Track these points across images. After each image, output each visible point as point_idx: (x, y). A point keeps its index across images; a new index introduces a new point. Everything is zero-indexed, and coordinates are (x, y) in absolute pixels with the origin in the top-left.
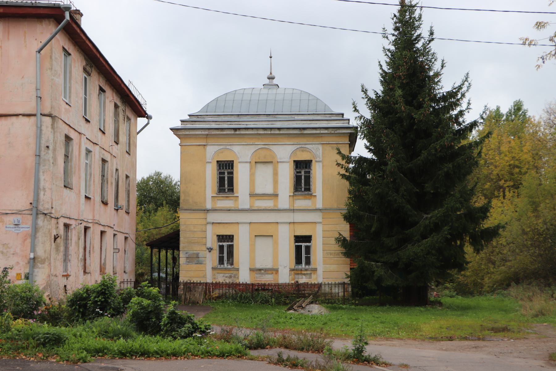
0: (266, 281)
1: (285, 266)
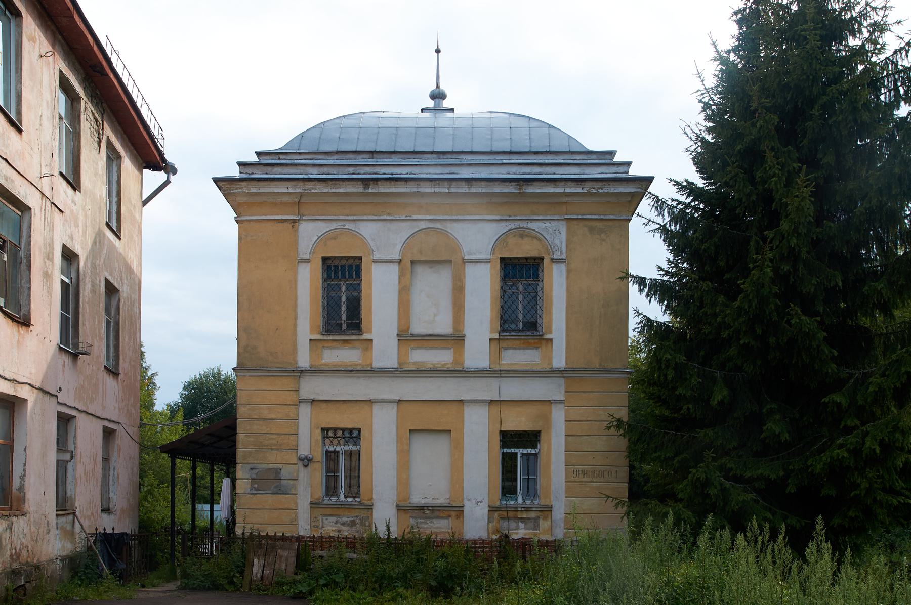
1: (478, 500)
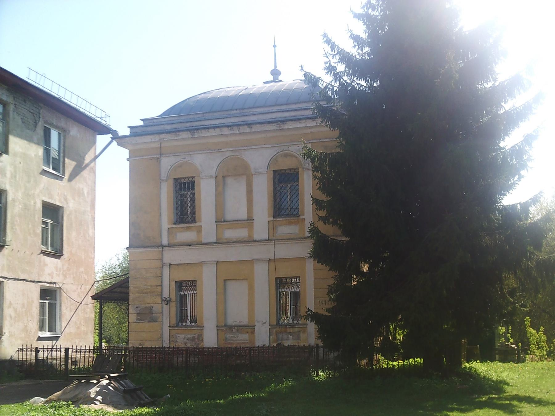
0: (239, 343)
1: (264, 322)
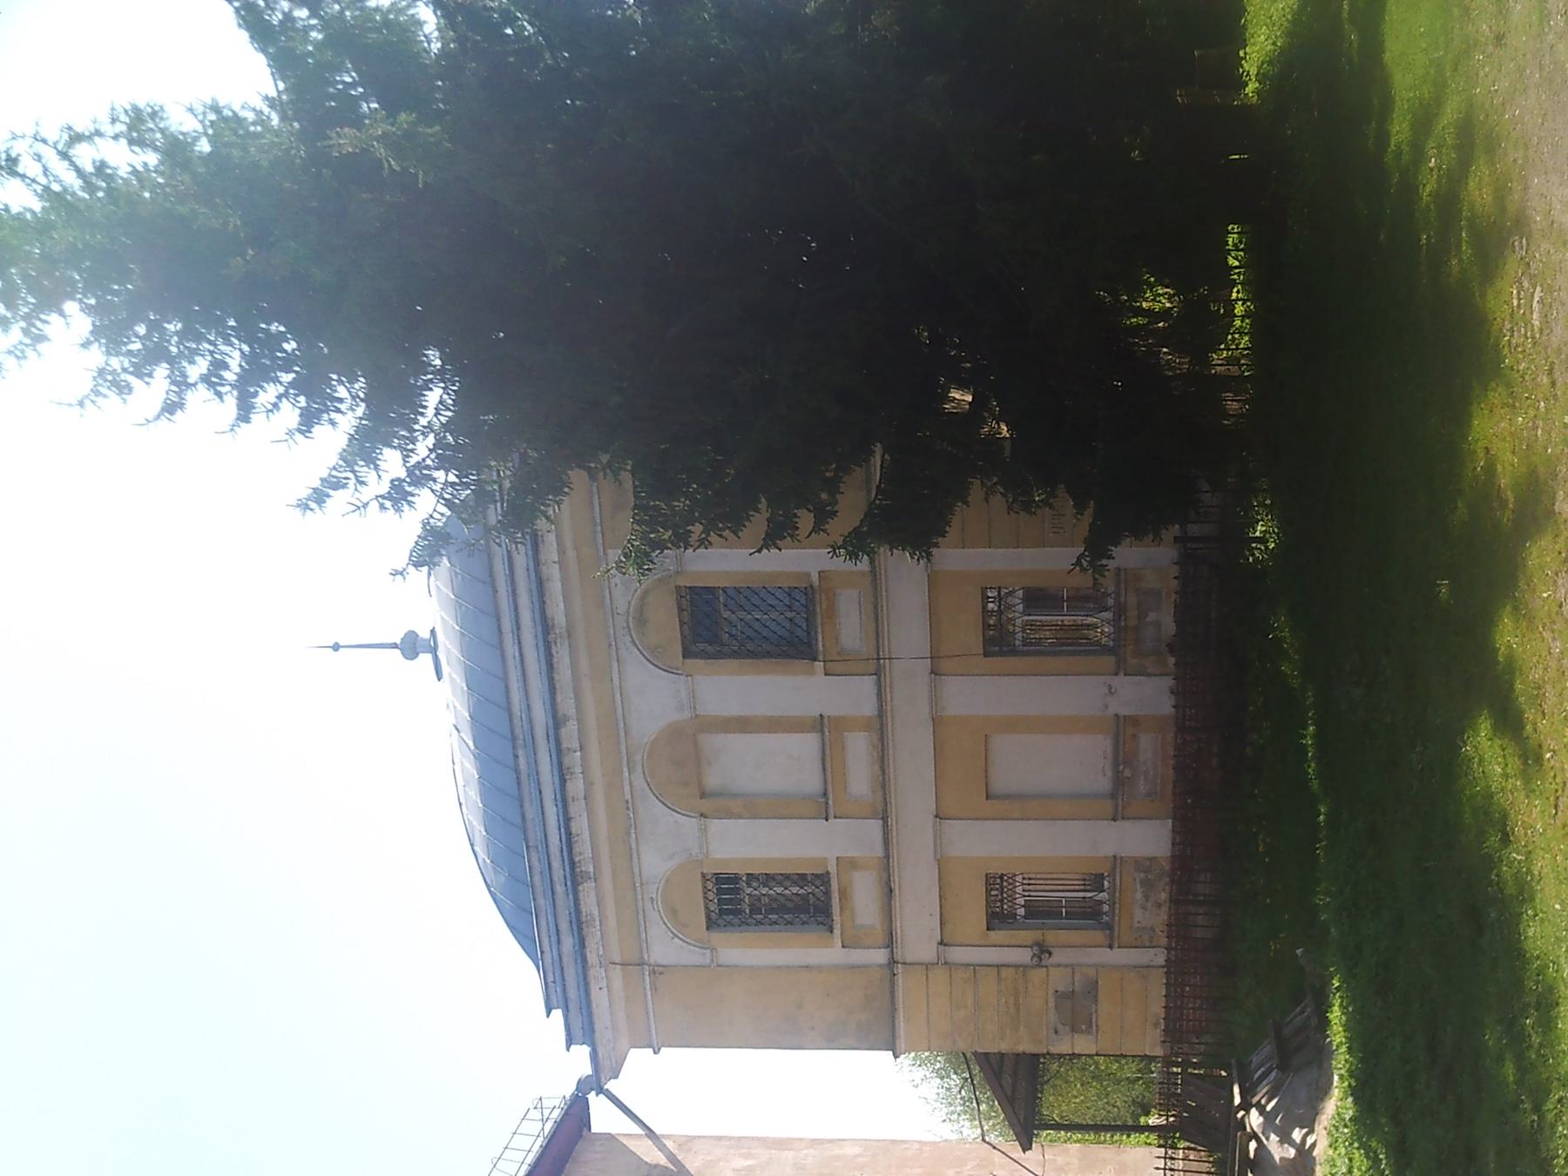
1: (1107, 691)
